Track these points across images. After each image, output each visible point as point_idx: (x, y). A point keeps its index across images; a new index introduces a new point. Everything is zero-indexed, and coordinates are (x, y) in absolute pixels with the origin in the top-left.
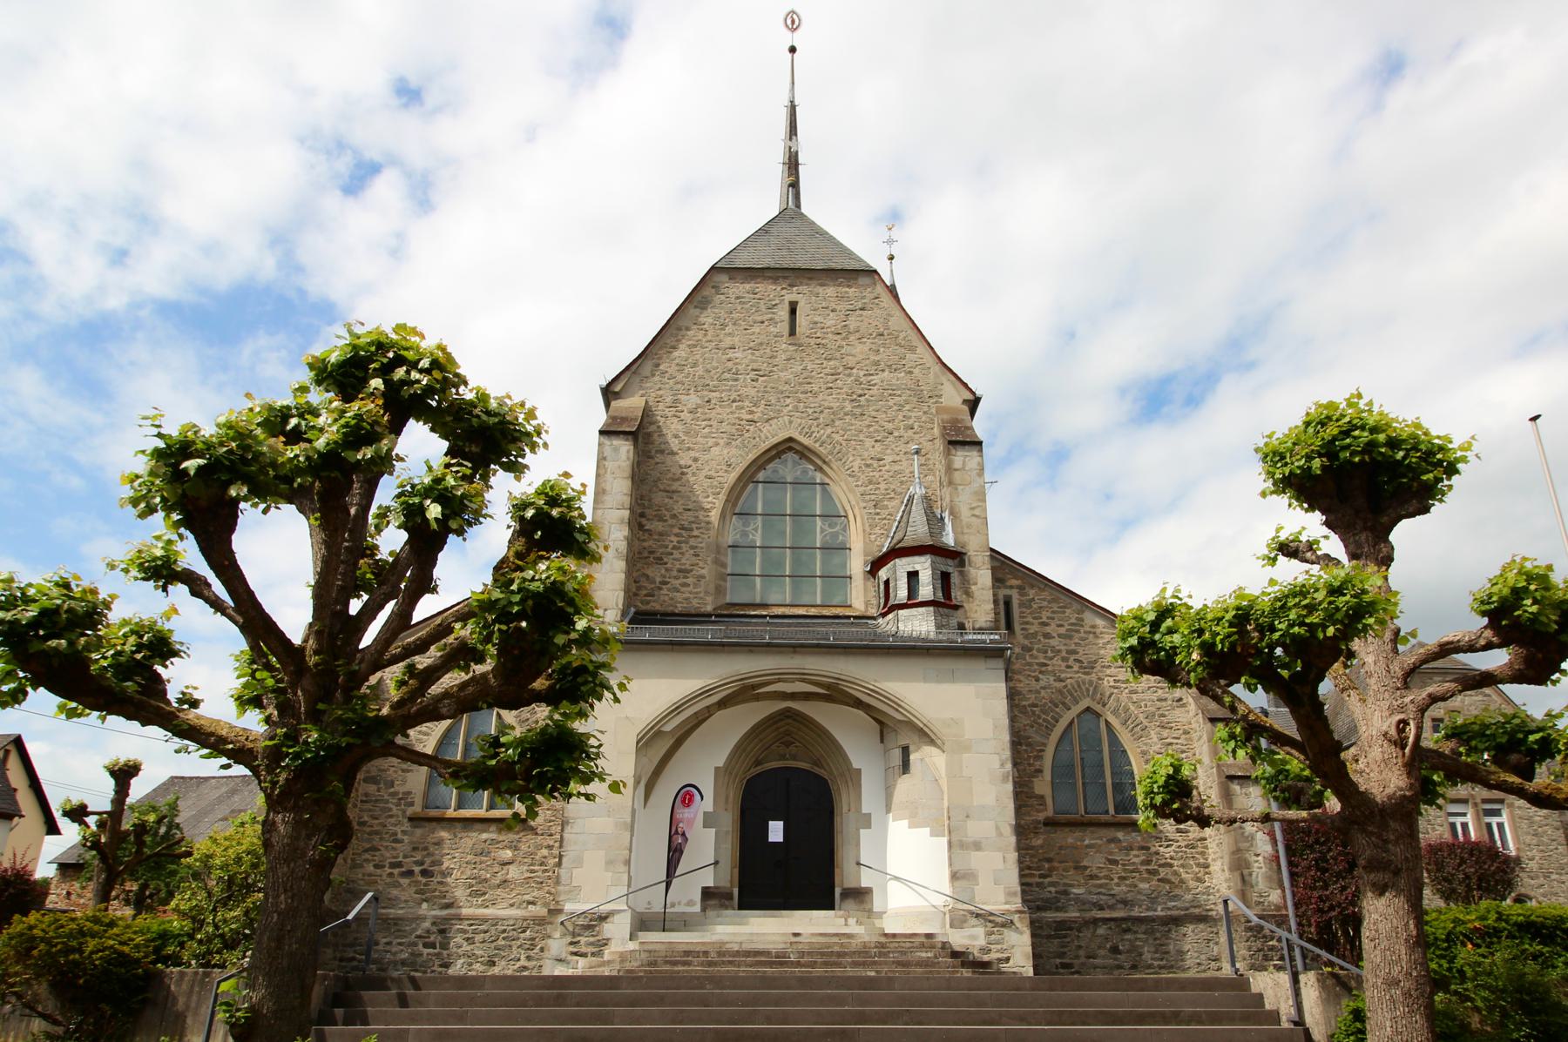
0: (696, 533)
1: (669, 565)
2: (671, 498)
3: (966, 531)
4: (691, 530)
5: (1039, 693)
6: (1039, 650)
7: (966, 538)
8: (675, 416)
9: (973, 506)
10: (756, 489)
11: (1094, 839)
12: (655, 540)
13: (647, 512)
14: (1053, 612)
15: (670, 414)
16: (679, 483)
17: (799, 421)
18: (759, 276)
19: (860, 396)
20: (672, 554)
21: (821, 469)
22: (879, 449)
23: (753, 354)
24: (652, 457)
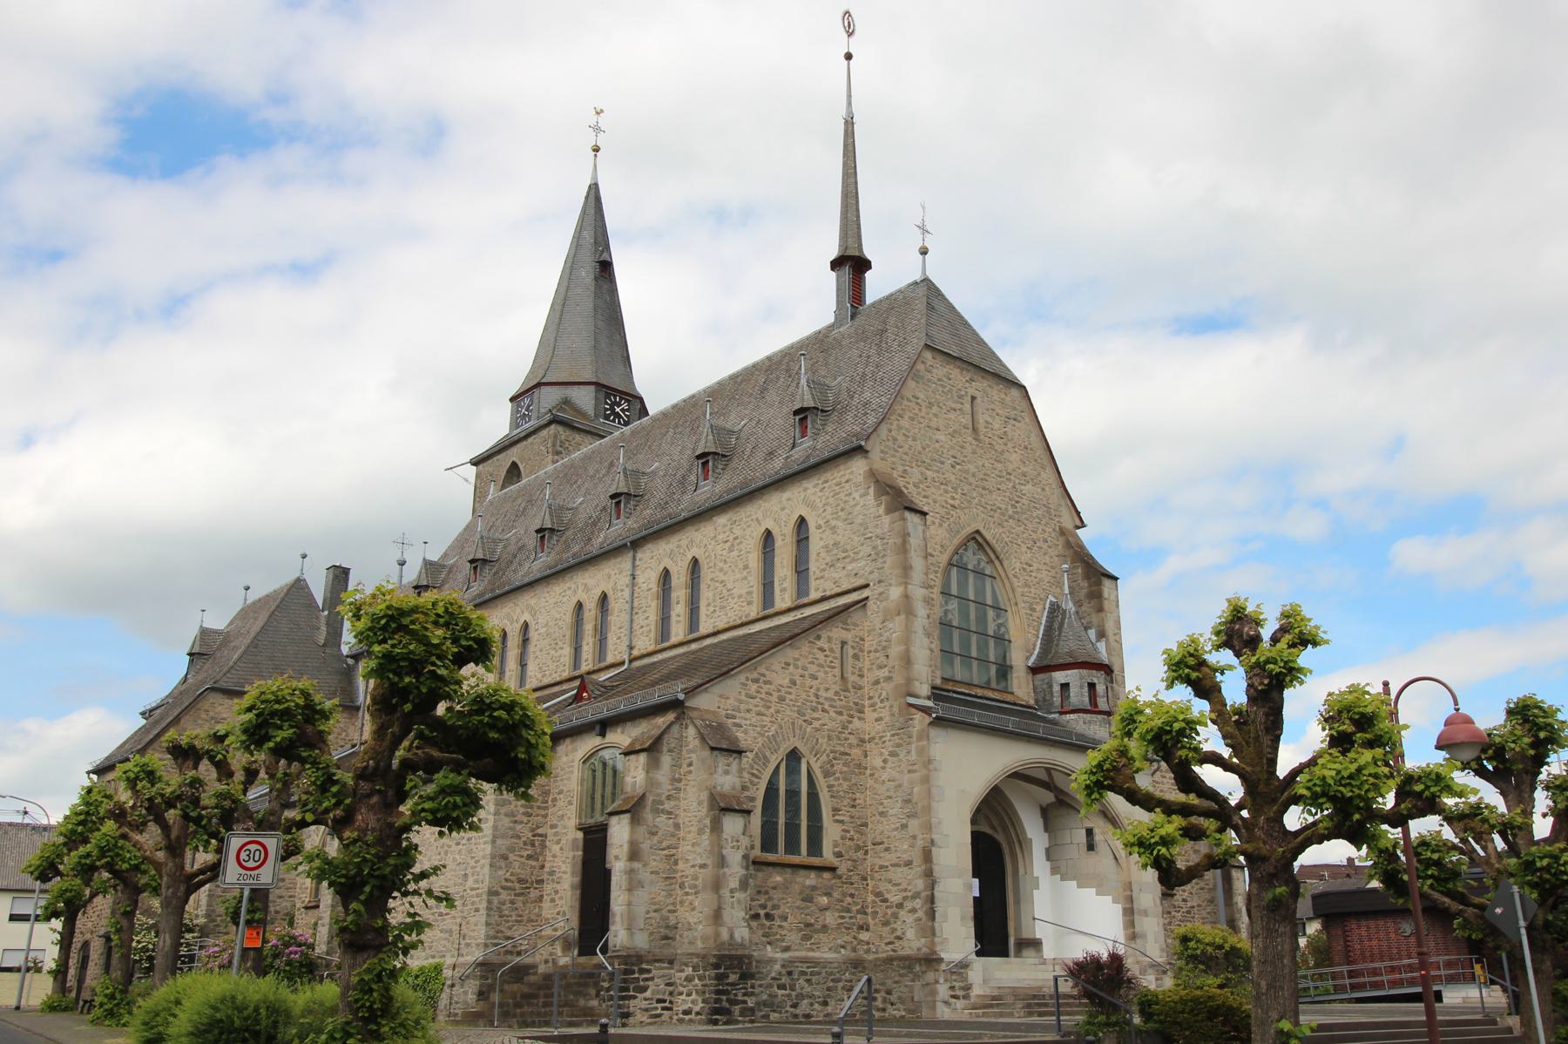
21: (991, 561)
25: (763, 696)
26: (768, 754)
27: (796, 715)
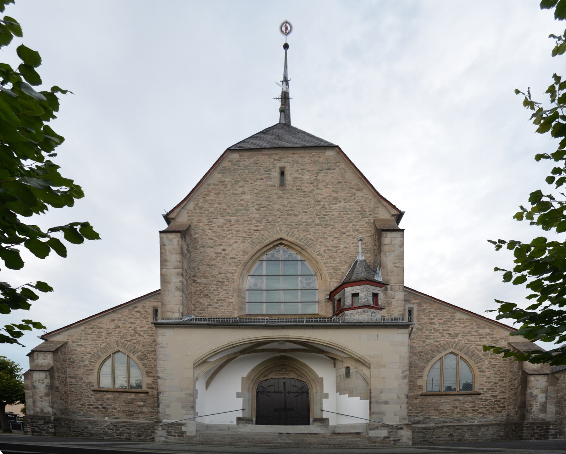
0: (226, 283)
1: (211, 298)
2: (210, 268)
3: (389, 274)
4: (224, 282)
5: (425, 347)
6: (426, 330)
7: (389, 277)
8: (210, 229)
9: (395, 262)
10: (261, 265)
11: (446, 400)
12: (203, 287)
13: (197, 274)
14: (437, 314)
15: (206, 228)
16: (215, 261)
17: (286, 229)
18: (259, 154)
19: (325, 215)
20: (213, 293)
22: (337, 242)
23: (256, 196)
24: (198, 250)
25: (97, 333)
26: (100, 354)
27: (120, 339)
